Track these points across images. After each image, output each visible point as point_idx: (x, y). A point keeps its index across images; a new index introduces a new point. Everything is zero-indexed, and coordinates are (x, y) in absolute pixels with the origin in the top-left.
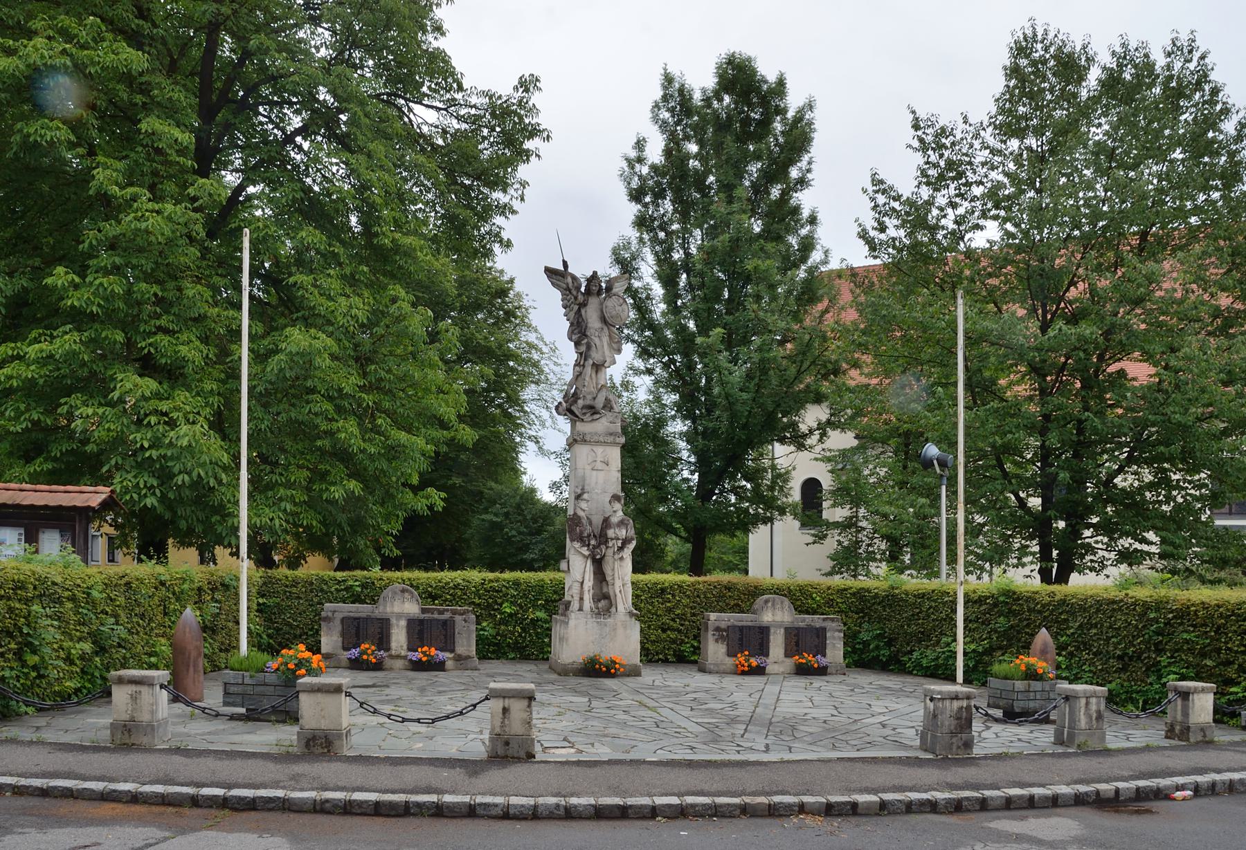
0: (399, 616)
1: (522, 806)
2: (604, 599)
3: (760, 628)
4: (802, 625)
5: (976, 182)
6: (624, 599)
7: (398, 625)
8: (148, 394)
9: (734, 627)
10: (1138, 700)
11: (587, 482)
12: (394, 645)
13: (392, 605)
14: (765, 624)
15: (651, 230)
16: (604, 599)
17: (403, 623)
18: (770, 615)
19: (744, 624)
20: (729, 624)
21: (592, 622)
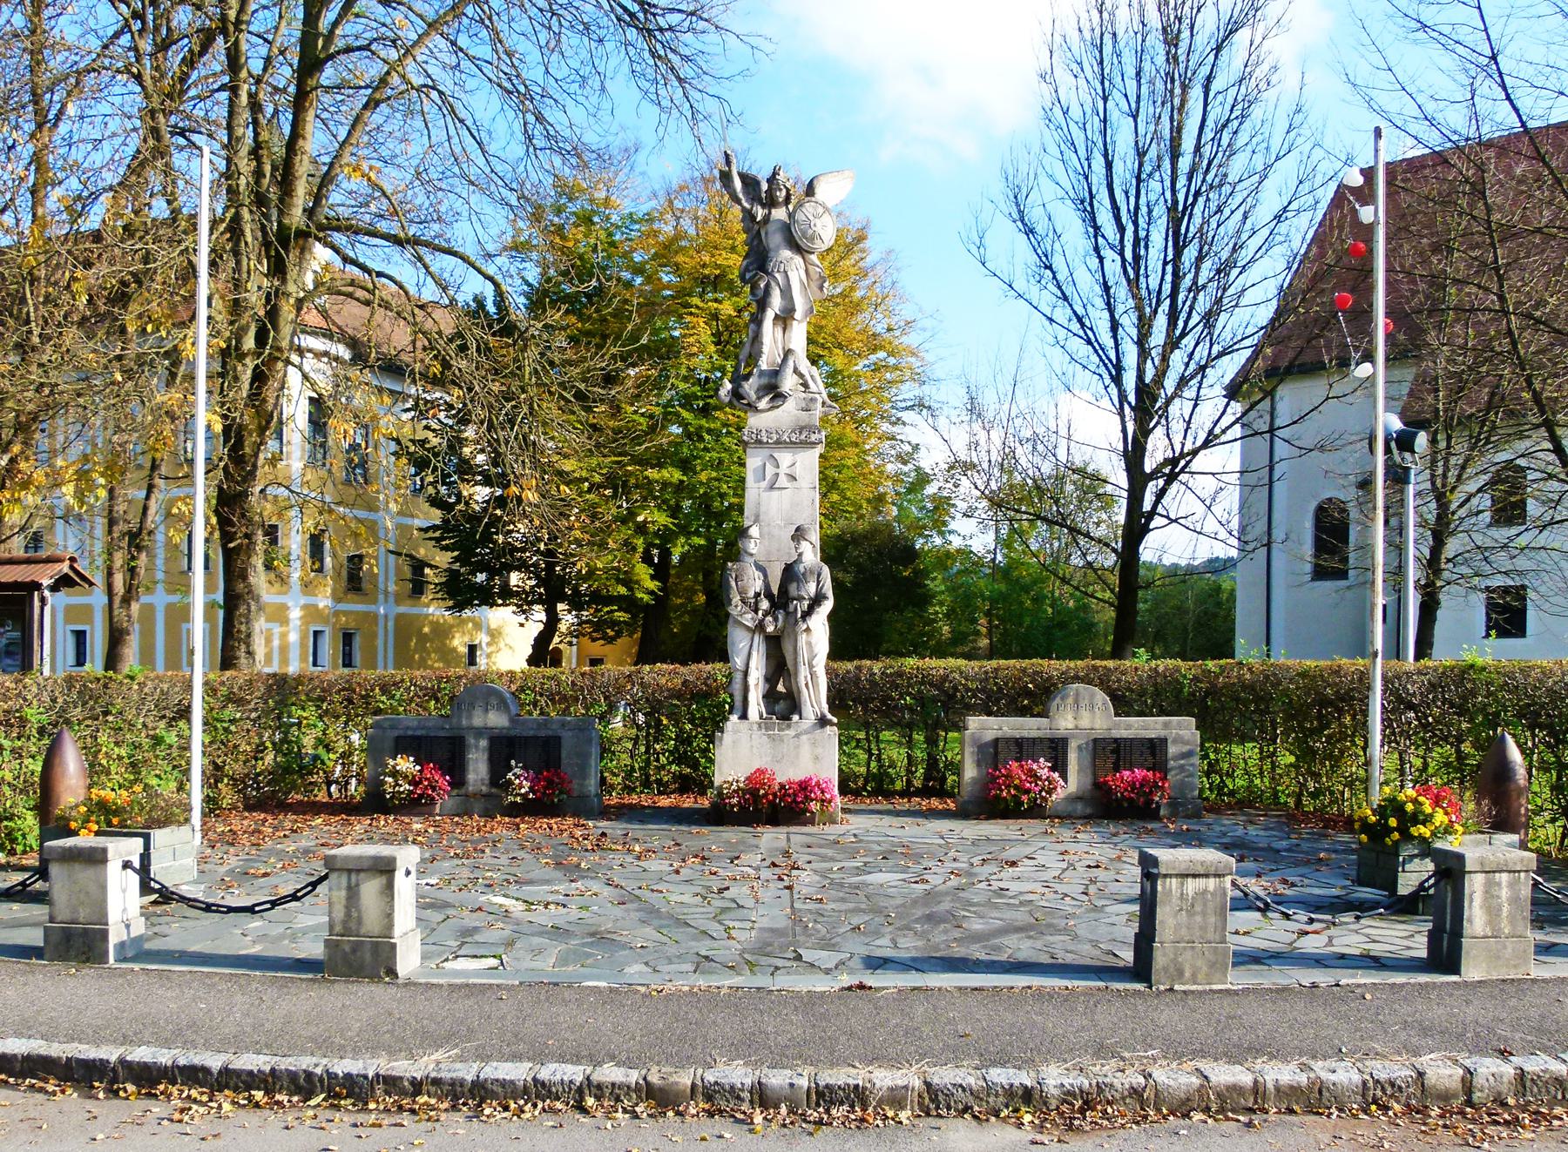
0: (479, 732)
1: (360, 858)
2: (783, 704)
3: (1052, 740)
4: (1124, 734)
5: (365, 107)
6: (815, 696)
7: (477, 747)
8: (387, 400)
9: (1008, 740)
10: (284, 608)
11: (763, 509)
12: (471, 777)
13: (470, 717)
14: (1061, 733)
15: (173, 193)
16: (783, 704)
17: (484, 743)
18: (1070, 717)
19: (1026, 734)
20: (999, 734)
21: (760, 738)
